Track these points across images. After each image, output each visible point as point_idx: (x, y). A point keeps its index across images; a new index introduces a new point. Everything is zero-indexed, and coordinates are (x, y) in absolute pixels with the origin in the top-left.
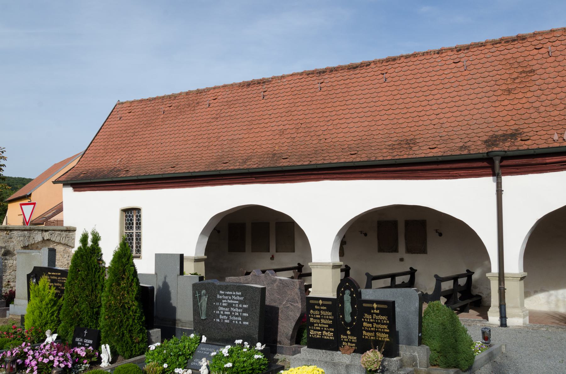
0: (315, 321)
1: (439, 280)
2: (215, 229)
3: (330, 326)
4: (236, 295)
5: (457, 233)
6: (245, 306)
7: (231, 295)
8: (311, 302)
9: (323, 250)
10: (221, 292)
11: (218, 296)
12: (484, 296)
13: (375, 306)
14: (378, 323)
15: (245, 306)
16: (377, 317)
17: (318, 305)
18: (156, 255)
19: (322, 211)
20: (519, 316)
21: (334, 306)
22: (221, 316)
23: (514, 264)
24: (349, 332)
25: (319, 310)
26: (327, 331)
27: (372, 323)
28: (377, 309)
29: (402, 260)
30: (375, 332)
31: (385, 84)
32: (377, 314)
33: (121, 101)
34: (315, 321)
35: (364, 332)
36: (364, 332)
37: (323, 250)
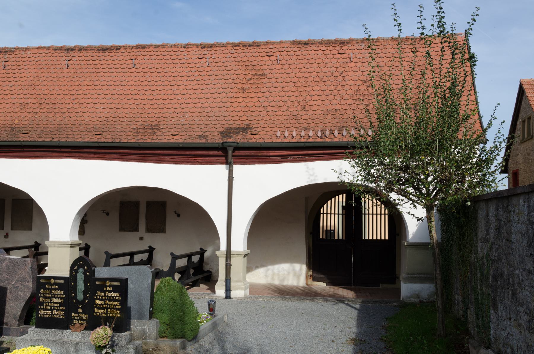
1: (175, 258)
3: (61, 305)
5: (193, 214)
9: (61, 228)
13: (108, 283)
14: (110, 300)
17: (50, 284)
20: (241, 289)
25: (50, 289)
26: (57, 310)
27: (104, 300)
28: (110, 286)
29: (141, 239)
30: (107, 308)
31: (134, 70)
32: (110, 292)
35: (96, 310)
36: (96, 310)
37: (61, 228)
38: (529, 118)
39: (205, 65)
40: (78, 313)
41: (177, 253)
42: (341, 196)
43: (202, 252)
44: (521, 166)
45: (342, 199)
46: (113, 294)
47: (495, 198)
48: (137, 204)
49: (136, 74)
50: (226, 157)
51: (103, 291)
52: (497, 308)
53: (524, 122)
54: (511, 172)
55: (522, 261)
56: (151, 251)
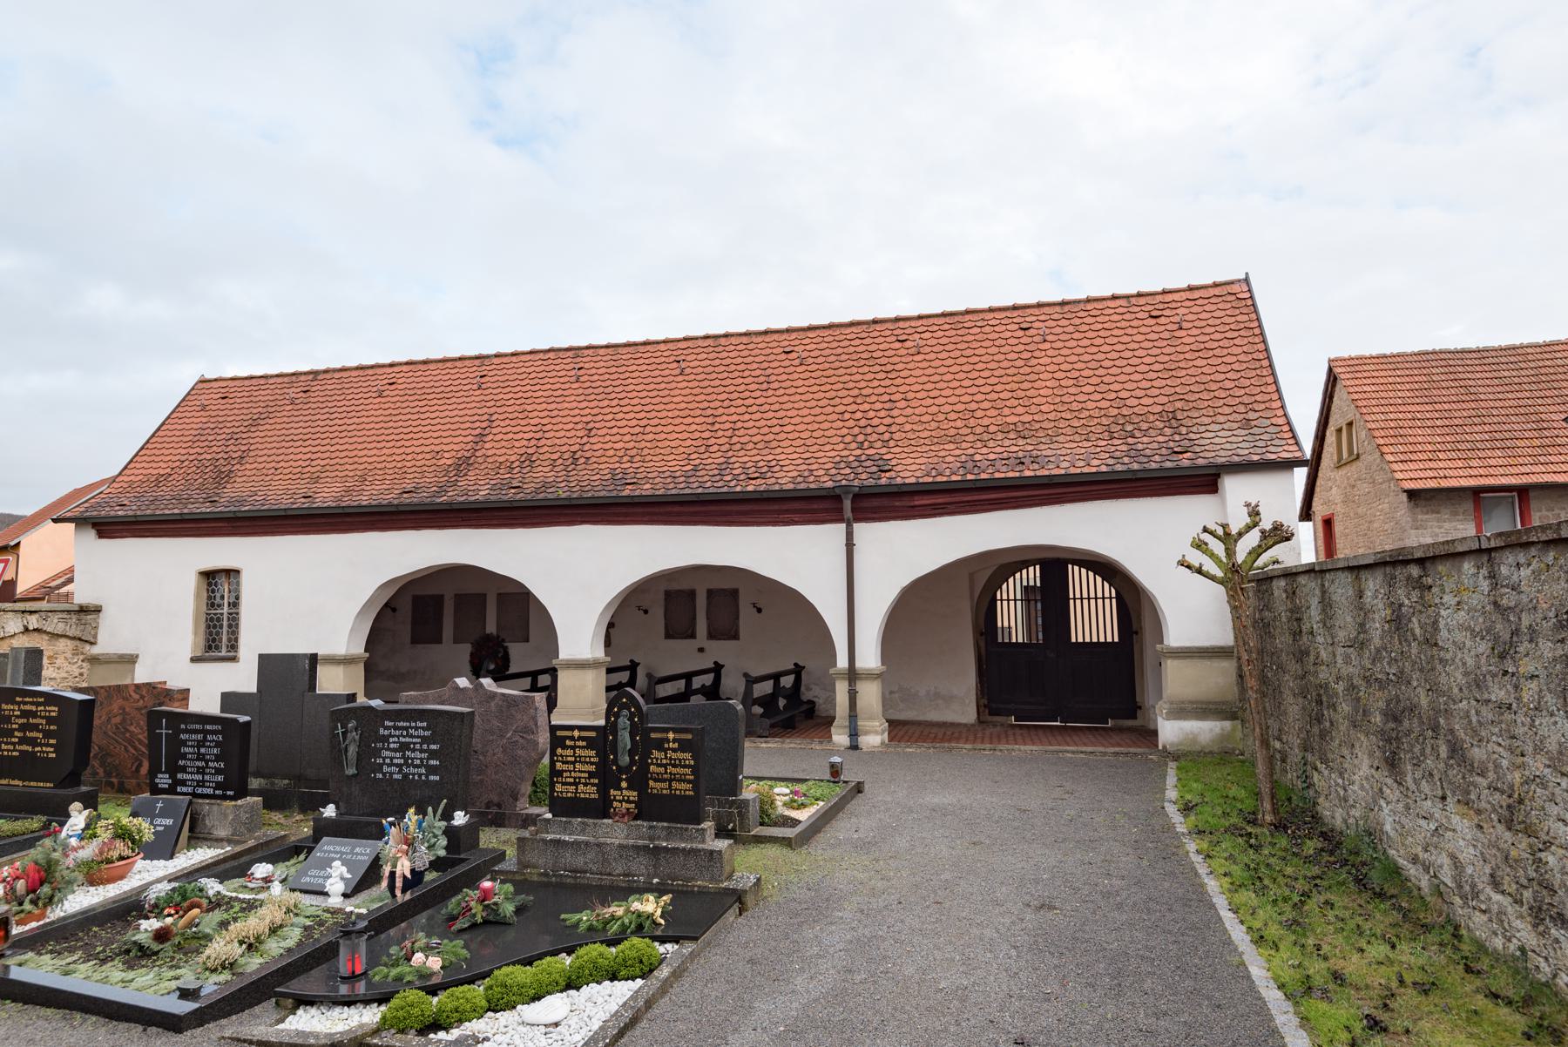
0: (565, 767)
1: (751, 681)
2: (386, 605)
3: (591, 775)
4: (417, 728)
5: (792, 607)
6: (433, 747)
7: (406, 728)
8: (559, 733)
9: (578, 635)
10: (387, 723)
11: (382, 731)
12: (819, 701)
13: (671, 736)
14: (674, 766)
15: (433, 747)
16: (674, 756)
17: (572, 738)
18: (261, 656)
19: (579, 578)
20: (876, 733)
21: (602, 739)
22: (385, 769)
23: (869, 657)
24: (624, 784)
25: (573, 748)
26: (585, 785)
27: (665, 766)
28: (674, 741)
29: (701, 650)
30: (670, 781)
31: (680, 378)
32: (674, 750)
33: (208, 376)
34: (565, 767)
35: (651, 783)
36: (651, 783)
37: (578, 635)
38: (1350, 424)
39: (797, 362)
40: (621, 789)
41: (755, 674)
42: (1031, 569)
43: (798, 670)
44: (1339, 510)
45: (1032, 575)
46: (680, 755)
47: (1385, 564)
48: (438, 600)
49: (685, 384)
50: (841, 510)
51: (661, 748)
52: (1403, 774)
53: (1339, 431)
54: (1318, 518)
55: (1479, 684)
56: (717, 669)
